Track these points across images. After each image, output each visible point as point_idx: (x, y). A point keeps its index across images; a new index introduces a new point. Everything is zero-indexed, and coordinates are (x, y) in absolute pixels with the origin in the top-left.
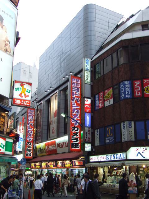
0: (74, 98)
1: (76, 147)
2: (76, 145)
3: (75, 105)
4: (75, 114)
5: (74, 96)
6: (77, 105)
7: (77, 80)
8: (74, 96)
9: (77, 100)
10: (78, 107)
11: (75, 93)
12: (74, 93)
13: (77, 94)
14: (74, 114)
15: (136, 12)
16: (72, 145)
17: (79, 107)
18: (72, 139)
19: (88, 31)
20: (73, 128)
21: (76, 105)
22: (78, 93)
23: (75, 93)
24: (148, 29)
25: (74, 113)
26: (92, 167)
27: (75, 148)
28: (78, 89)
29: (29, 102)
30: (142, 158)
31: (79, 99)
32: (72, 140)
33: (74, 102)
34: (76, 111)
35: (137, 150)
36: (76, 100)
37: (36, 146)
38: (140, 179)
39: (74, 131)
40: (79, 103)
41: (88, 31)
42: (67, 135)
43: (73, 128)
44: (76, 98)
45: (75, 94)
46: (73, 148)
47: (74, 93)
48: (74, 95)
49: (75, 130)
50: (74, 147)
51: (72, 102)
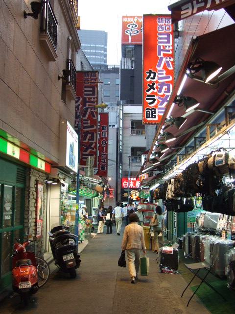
1: (152, 117)
2: (152, 112)
3: (163, 74)
4: (164, 95)
5: (162, 56)
6: (166, 74)
7: (165, 21)
9: (168, 62)
10: (169, 78)
11: (163, 46)
13: (167, 48)
14: (161, 96)
15: (4, 162)
16: (147, 112)
17: (171, 79)
18: (147, 99)
20: (148, 74)
21: (164, 75)
22: (169, 47)
24: (124, 17)
25: (162, 93)
26: (186, 169)
27: (151, 119)
28: (168, 38)
29: (85, 125)
31: (172, 60)
32: (147, 101)
33: (161, 68)
34: (165, 87)
36: (165, 64)
37: (107, 115)
39: (149, 80)
40: (171, 68)
43: (148, 74)
45: (163, 50)
47: (162, 48)
49: (151, 78)
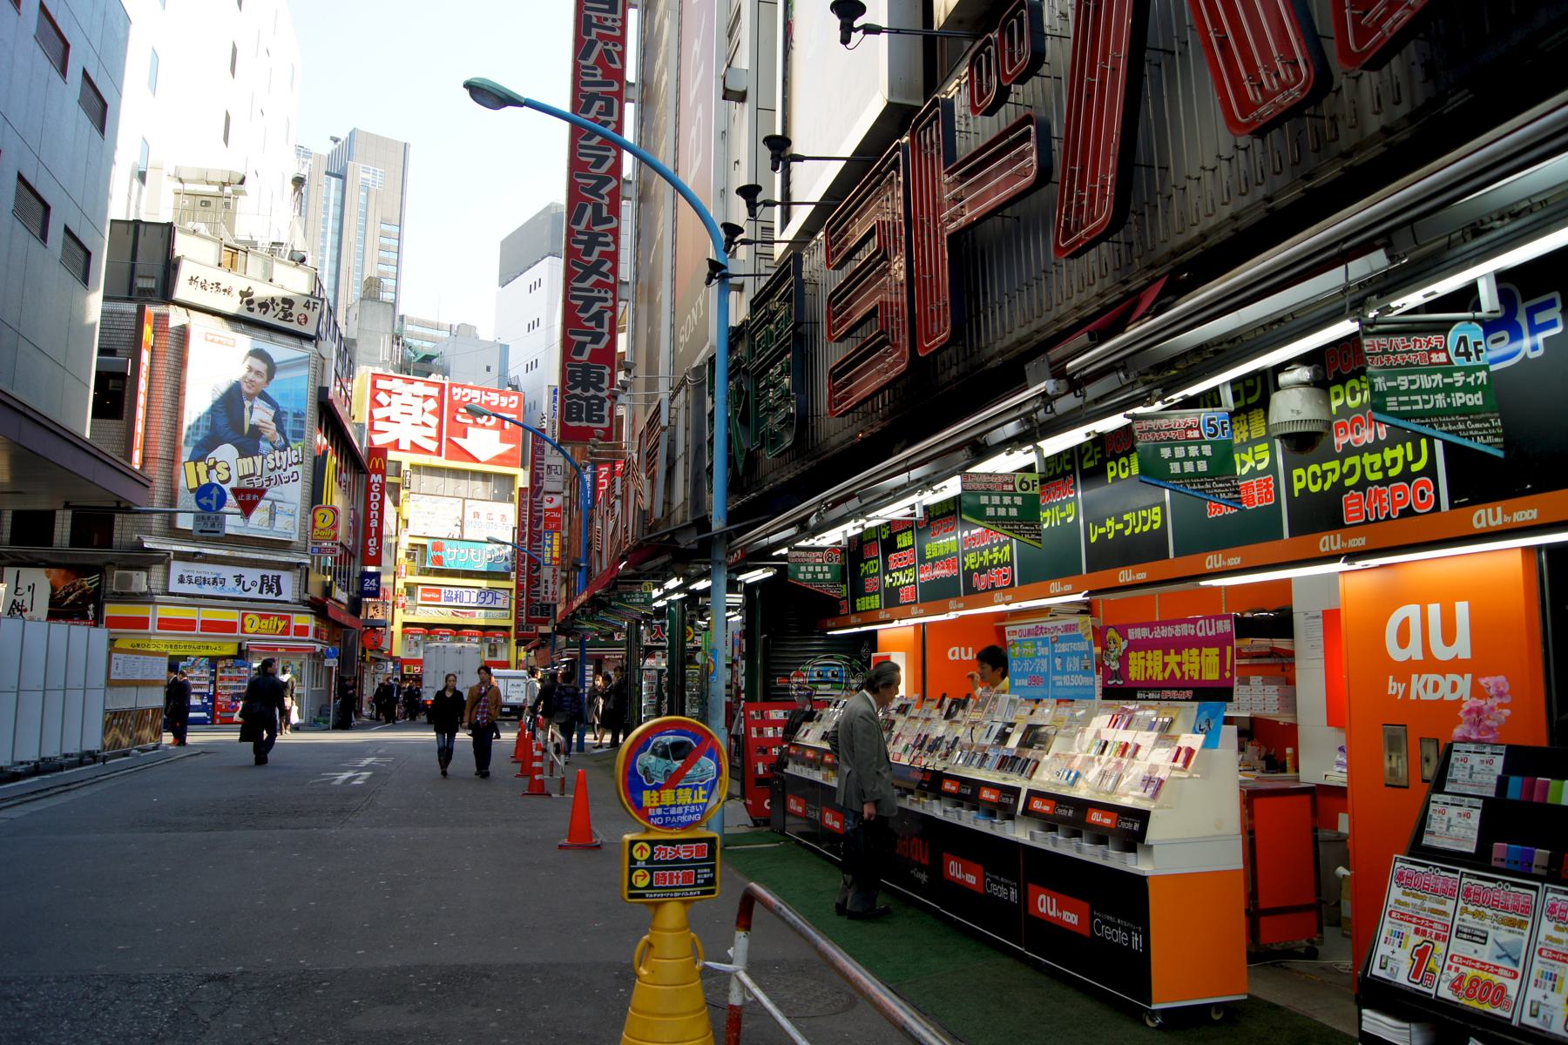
0: (592, 44)
1: (589, 420)
5: (593, 37)
8: (593, 37)
11: (599, 18)
12: (594, 21)
13: (609, 23)
19: (890, 31)
21: (599, 78)
22: (614, 20)
23: (599, 18)
27: (584, 424)
30: (669, 167)
35: (488, 369)
38: (856, 30)
41: (890, 31)
42: (1551, 741)
44: (600, 45)
45: (596, 26)
46: (576, 424)
48: (594, 31)
50: (581, 420)
51: (583, 62)
